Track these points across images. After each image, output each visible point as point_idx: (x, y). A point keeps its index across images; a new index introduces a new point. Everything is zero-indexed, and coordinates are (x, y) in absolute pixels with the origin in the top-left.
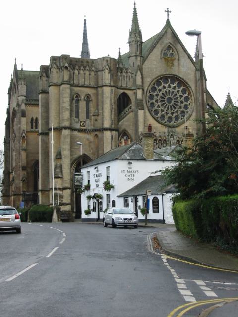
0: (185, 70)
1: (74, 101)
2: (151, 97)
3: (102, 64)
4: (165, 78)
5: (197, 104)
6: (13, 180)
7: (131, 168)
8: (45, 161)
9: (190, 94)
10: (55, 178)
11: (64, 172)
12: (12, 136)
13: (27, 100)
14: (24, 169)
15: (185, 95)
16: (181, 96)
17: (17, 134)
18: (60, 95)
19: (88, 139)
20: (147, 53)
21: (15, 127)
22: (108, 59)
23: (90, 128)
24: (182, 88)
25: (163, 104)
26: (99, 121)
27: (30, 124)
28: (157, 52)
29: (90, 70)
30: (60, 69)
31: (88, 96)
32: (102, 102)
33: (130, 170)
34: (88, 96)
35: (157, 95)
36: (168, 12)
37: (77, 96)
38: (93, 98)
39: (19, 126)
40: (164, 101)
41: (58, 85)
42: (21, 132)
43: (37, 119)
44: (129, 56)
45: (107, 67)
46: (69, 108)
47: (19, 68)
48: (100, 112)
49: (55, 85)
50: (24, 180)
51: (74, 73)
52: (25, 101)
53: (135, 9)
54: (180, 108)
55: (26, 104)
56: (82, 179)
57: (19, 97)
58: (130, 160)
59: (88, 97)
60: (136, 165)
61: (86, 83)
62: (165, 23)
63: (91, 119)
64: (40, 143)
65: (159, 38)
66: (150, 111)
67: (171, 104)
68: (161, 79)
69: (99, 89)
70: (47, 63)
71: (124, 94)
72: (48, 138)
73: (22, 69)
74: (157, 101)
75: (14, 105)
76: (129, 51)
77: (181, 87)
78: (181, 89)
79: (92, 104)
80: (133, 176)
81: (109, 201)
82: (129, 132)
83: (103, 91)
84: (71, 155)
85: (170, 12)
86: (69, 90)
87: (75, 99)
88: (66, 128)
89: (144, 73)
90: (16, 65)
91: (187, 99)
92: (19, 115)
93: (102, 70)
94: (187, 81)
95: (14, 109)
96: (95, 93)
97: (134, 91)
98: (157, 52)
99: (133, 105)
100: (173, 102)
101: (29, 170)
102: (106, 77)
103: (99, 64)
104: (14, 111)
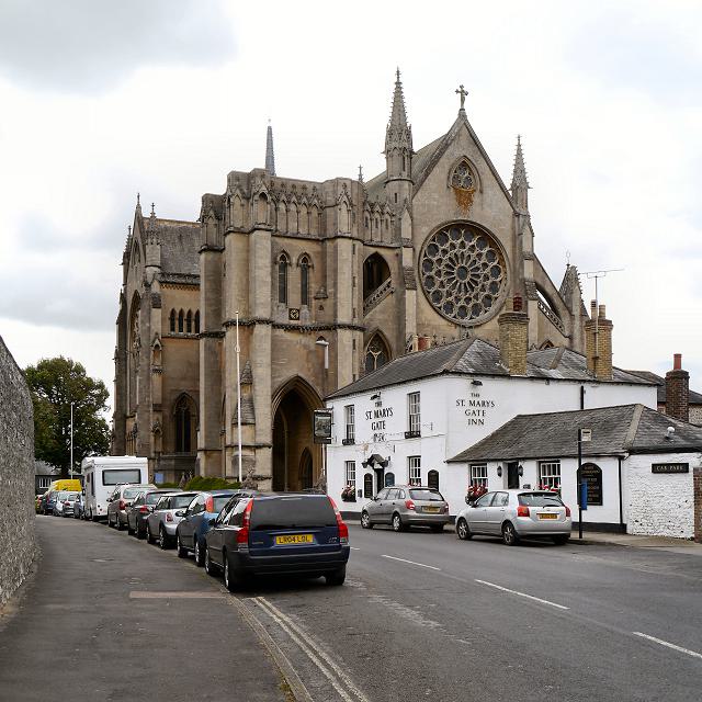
0: (489, 212)
1: (277, 267)
2: (428, 265)
3: (335, 192)
4: (457, 227)
5: (515, 281)
6: (136, 431)
7: (478, 395)
8: (212, 389)
9: (502, 261)
10: (242, 424)
11: (257, 412)
12: (131, 346)
13: (163, 275)
14: (157, 408)
15: (491, 265)
16: (485, 265)
17: (144, 342)
18: (248, 251)
19: (305, 346)
20: (421, 175)
21: (139, 330)
22: (348, 183)
23: (308, 323)
24: (488, 249)
25: (450, 280)
26: (328, 310)
27: (169, 322)
28: (440, 173)
29: (310, 205)
30: (248, 199)
31: (305, 258)
32: (335, 271)
33: (476, 399)
34: (305, 258)
35: (440, 261)
36: (463, 93)
37: (283, 258)
38: (315, 261)
39: (148, 325)
40: (453, 274)
41: (245, 233)
42: (152, 338)
43: (198, 313)
44: (384, 181)
45: (345, 198)
46: (269, 279)
47: (146, 214)
48: (330, 290)
49: (239, 232)
50: (158, 431)
51: (276, 209)
52: (159, 277)
53: (398, 83)
54: (483, 289)
55: (161, 283)
56: (330, 423)
57: (147, 269)
58: (477, 375)
59: (305, 260)
60: (490, 388)
61: (300, 230)
62: (455, 116)
63: (310, 307)
64: (202, 355)
65: (444, 144)
66: (426, 294)
67: (466, 280)
68: (447, 229)
69: (328, 244)
70: (220, 189)
71: (376, 256)
72: (220, 344)
73: (153, 213)
74: (439, 273)
75: (136, 285)
76: (384, 168)
77: (486, 246)
78: (484, 251)
79: (313, 276)
80: (481, 413)
81: (418, 473)
82: (385, 333)
83: (336, 247)
84: (273, 378)
85: (457, 92)
86: (269, 242)
87: (281, 262)
88: (261, 322)
89: (414, 216)
90: (139, 207)
91: (496, 271)
92: (146, 304)
93: (337, 205)
94: (493, 230)
95: (136, 292)
96: (318, 253)
97: (397, 251)
98: (440, 173)
99: (393, 280)
100: (469, 277)
101: (167, 412)
102: (343, 221)
103: (327, 193)
104: (136, 298)
